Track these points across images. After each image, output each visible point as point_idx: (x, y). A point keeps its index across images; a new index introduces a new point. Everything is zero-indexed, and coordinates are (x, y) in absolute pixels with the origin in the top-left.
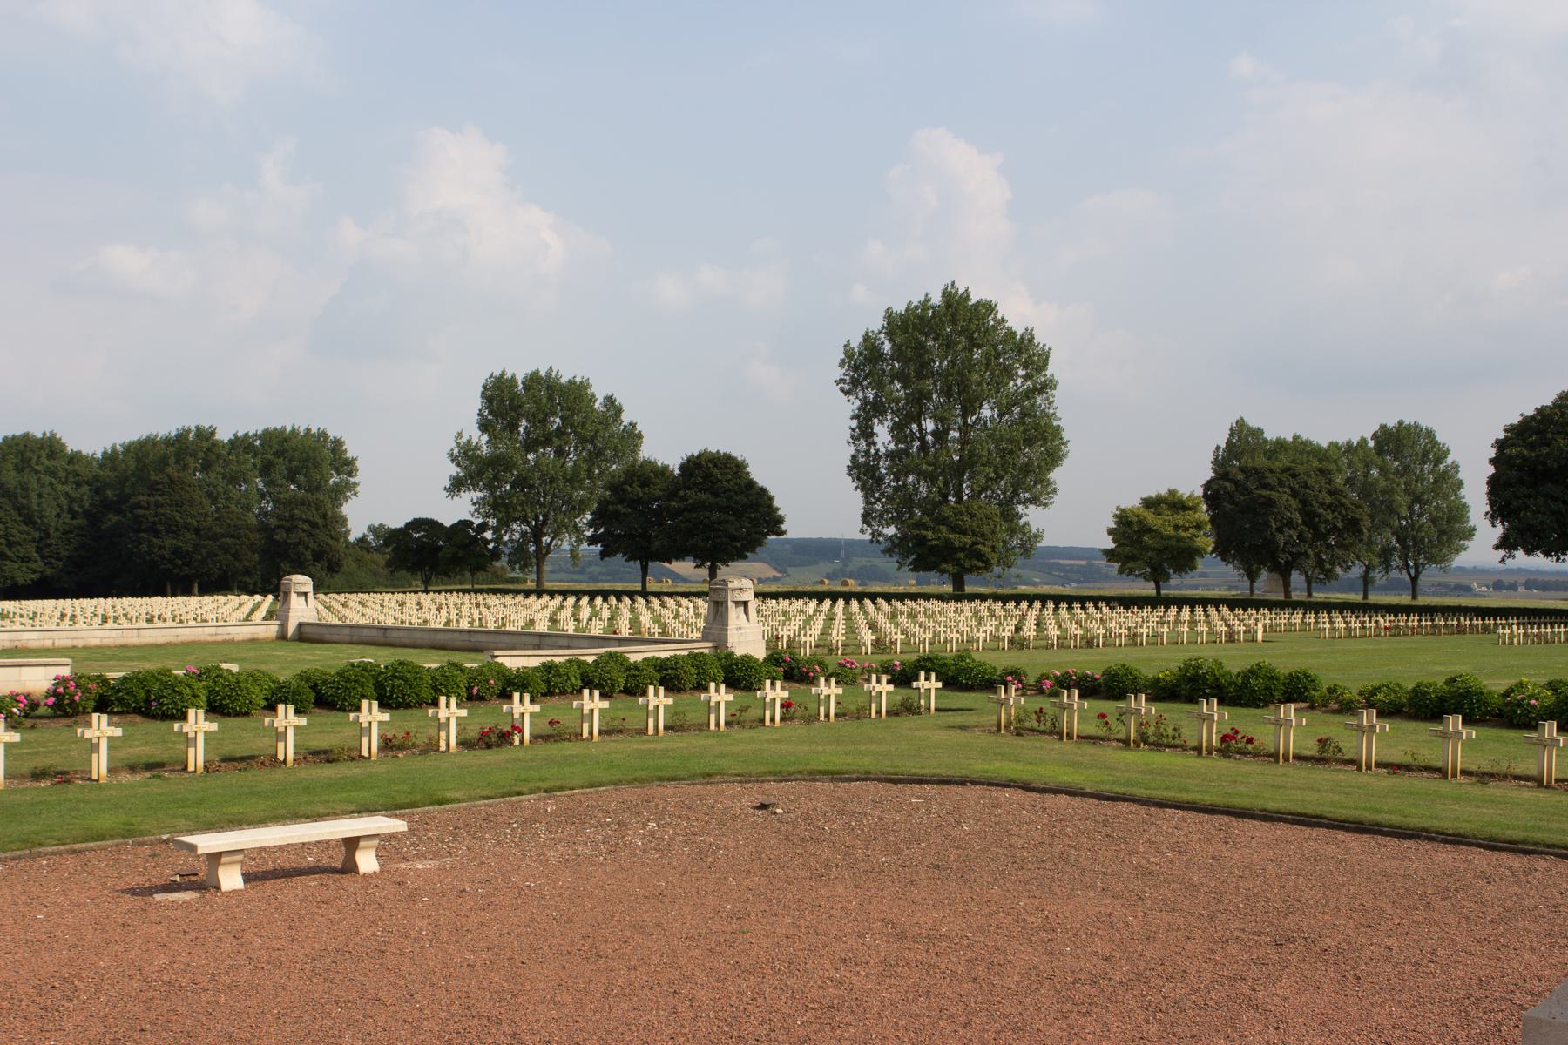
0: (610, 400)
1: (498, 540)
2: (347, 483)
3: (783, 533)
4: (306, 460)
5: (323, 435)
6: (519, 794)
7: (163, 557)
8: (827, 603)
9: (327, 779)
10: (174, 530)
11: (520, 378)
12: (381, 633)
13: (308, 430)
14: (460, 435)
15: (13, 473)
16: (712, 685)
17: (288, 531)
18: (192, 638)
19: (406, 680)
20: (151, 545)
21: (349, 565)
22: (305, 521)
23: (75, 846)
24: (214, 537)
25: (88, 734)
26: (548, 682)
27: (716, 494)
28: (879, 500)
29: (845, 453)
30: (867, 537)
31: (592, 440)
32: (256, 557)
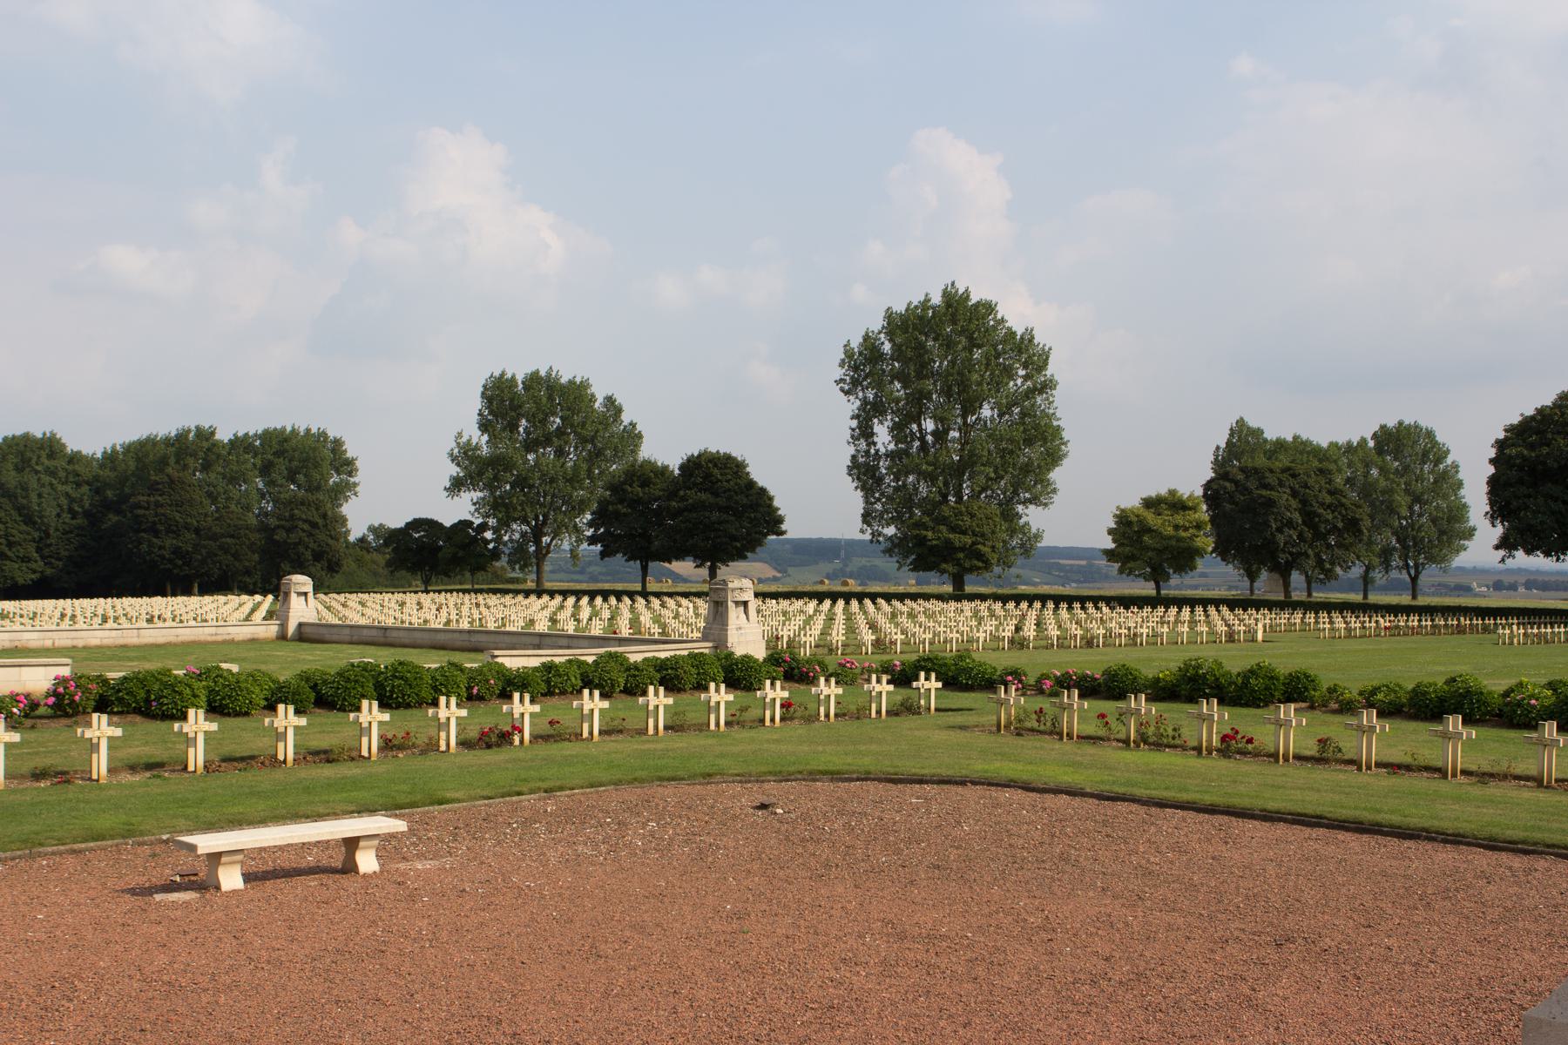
0: (610, 400)
1: (498, 540)
2: (347, 483)
3: (783, 533)
4: (306, 460)
5: (323, 435)
6: (519, 794)
7: (163, 557)
8: (827, 603)
9: (327, 779)
10: (174, 530)
11: (520, 378)
12: (381, 633)
13: (308, 430)
14: (460, 435)
15: (13, 473)
16: (712, 685)
17: (288, 531)
18: (192, 638)
19: (406, 680)
20: (151, 545)
21: (349, 565)
22: (305, 521)
23: (75, 846)
24: (214, 537)
25: (88, 734)
26: (548, 682)
27: (716, 494)
28: (879, 500)
29: (845, 453)
30: (867, 537)
31: (592, 440)
32: (256, 557)
